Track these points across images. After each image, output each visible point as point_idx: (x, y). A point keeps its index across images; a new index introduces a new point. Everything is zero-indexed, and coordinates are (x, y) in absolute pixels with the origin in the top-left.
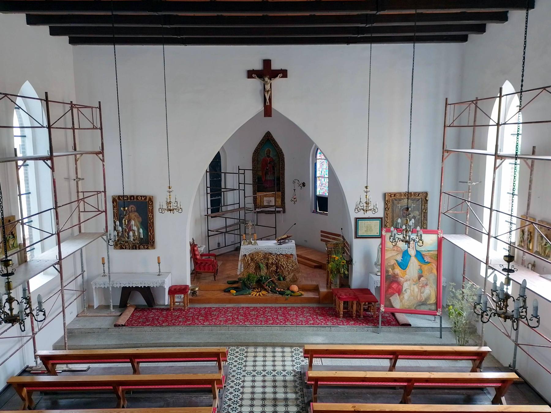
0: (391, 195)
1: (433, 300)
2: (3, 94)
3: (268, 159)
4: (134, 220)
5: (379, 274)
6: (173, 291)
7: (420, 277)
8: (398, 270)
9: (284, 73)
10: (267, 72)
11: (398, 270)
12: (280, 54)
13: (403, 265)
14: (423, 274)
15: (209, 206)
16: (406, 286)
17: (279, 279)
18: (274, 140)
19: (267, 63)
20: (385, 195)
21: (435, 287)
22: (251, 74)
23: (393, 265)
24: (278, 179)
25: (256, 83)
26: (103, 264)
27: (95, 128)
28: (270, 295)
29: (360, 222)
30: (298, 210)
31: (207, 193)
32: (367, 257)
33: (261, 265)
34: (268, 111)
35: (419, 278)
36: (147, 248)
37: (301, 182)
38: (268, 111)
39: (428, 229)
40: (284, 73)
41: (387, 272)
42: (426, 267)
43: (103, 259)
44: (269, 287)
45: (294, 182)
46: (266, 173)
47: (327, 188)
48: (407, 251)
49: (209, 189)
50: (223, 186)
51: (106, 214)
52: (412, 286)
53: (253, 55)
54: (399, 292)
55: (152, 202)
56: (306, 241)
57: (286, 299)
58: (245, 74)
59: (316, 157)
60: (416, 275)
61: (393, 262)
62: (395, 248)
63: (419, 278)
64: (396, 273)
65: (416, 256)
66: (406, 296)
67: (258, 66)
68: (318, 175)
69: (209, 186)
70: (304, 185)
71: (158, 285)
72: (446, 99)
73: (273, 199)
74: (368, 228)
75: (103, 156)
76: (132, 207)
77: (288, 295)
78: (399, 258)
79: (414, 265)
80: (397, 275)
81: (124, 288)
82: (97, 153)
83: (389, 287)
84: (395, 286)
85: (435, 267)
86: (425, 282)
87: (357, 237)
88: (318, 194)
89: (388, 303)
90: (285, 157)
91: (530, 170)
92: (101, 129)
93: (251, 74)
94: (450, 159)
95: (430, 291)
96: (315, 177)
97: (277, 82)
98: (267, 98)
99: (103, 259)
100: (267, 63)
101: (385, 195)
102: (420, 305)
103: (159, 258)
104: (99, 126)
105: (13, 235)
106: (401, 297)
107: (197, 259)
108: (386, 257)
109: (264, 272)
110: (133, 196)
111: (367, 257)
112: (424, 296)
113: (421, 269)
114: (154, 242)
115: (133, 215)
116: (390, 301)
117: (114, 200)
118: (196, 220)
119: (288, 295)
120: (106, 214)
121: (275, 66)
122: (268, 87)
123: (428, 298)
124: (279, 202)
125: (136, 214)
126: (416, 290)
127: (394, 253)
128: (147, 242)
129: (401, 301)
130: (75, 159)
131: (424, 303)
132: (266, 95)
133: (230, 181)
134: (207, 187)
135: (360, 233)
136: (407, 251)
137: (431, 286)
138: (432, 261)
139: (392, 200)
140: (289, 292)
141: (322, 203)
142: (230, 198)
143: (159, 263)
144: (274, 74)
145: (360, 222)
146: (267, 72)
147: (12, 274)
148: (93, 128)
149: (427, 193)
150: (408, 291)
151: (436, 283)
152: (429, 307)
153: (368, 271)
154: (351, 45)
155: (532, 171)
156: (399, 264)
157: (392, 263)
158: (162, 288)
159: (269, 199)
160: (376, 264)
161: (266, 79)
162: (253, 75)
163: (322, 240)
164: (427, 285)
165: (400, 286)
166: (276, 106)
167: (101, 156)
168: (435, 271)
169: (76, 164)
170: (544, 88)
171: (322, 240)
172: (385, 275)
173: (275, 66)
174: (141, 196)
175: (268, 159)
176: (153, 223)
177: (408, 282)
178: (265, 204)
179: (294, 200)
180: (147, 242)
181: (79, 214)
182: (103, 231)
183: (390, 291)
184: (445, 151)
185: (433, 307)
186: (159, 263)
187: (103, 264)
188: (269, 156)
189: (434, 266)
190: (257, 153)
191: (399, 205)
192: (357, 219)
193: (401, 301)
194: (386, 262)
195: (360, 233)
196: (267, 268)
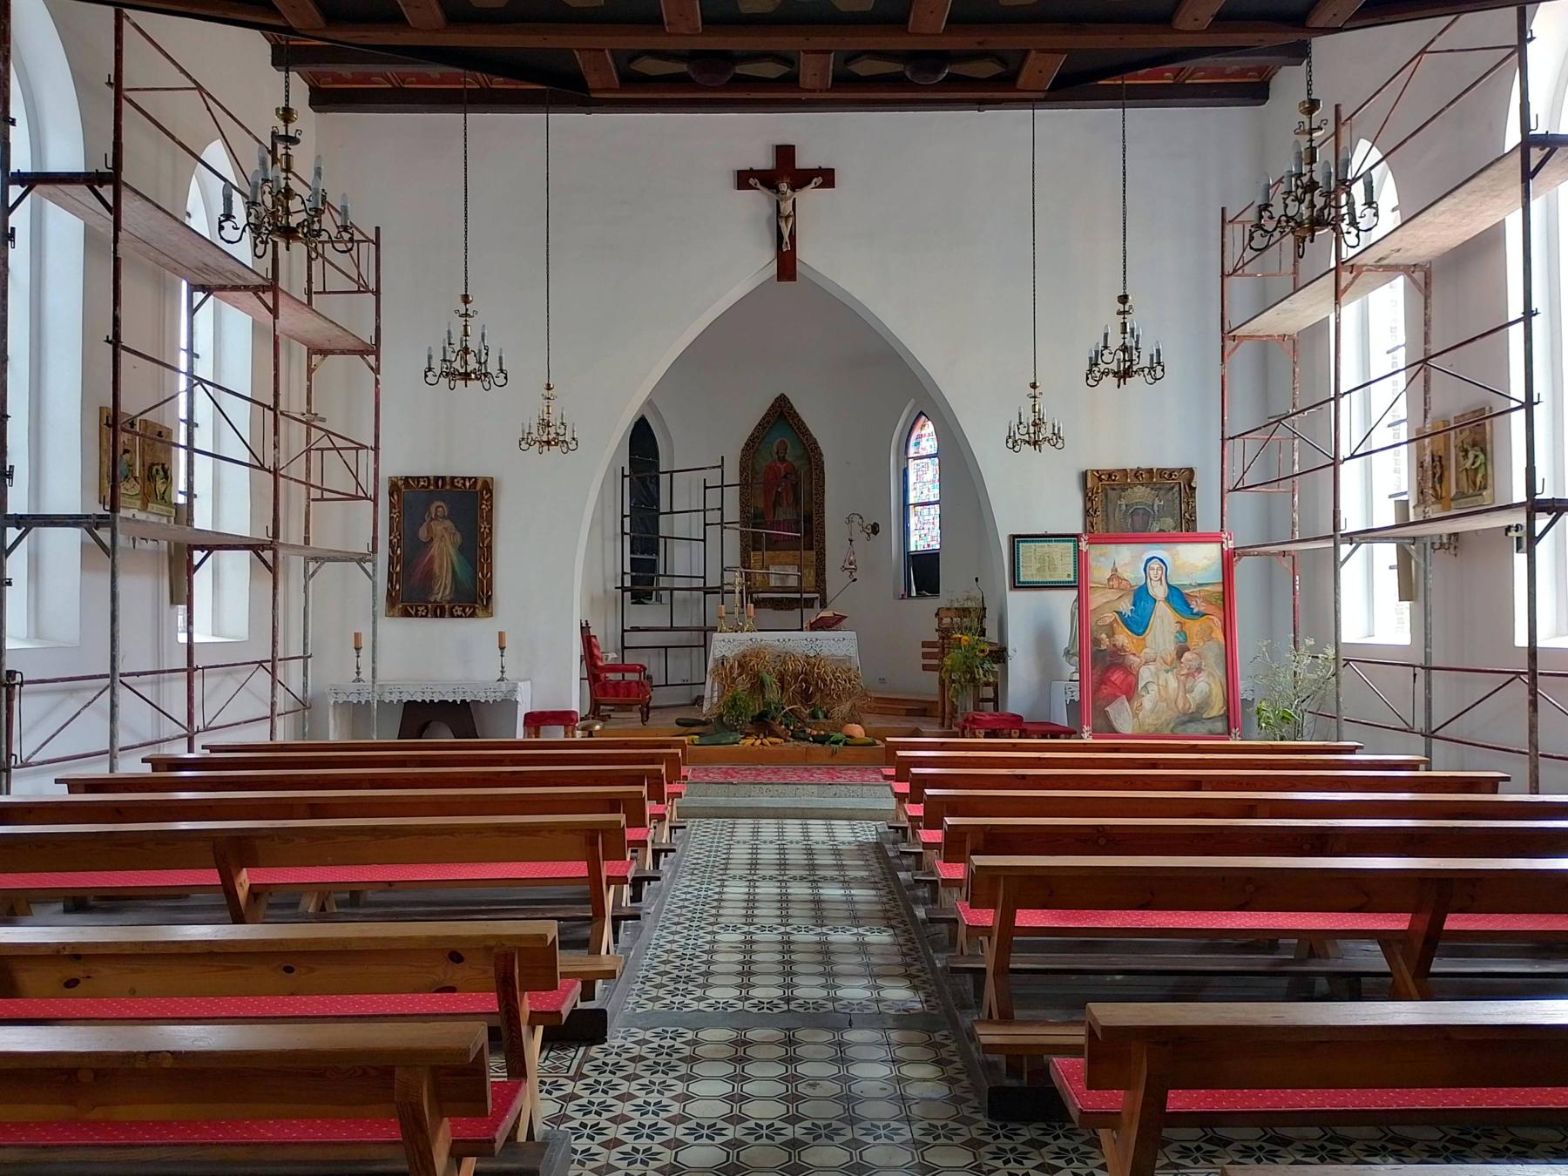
0: (1099, 475)
1: (1217, 708)
2: (195, 82)
3: (782, 467)
4: (441, 545)
5: (1077, 677)
6: (535, 720)
7: (1181, 651)
8: (1123, 638)
9: (827, 178)
10: (784, 174)
11: (1123, 638)
12: (816, 134)
13: (1138, 624)
14: (1190, 644)
15: (627, 569)
16: (1145, 674)
17: (814, 716)
18: (796, 416)
19: (785, 153)
20: (1084, 475)
21: (1220, 673)
22: (744, 179)
23: (1111, 625)
24: (808, 519)
25: (757, 201)
26: (358, 649)
27: (362, 289)
28: (792, 744)
29: (1023, 547)
30: (862, 585)
31: (623, 533)
32: (1044, 639)
33: (768, 679)
34: (787, 265)
35: (1180, 655)
36: (472, 615)
37: (869, 521)
38: (787, 265)
39: (1199, 530)
40: (827, 178)
41: (1097, 642)
42: (1194, 627)
43: (357, 636)
44: (787, 726)
45: (849, 520)
46: (776, 504)
47: (937, 531)
48: (1144, 588)
49: (627, 520)
50: (664, 507)
51: (376, 505)
52: (1163, 676)
53: (750, 135)
54: (1130, 690)
55: (491, 492)
56: (882, 680)
57: (834, 753)
58: (731, 180)
59: (906, 452)
60: (1171, 648)
61: (1110, 617)
62: (1115, 583)
63: (1180, 655)
64: (1119, 644)
65: (1167, 599)
66: (1147, 701)
67: (765, 162)
68: (912, 500)
69: (627, 512)
70: (875, 529)
71: (499, 697)
72: (1223, 209)
73: (792, 570)
74: (1046, 563)
75: (378, 359)
76: (439, 507)
77: (837, 742)
78: (1126, 606)
79: (1164, 621)
80: (1123, 648)
81: (410, 705)
82: (363, 352)
83: (1103, 681)
84: (1117, 677)
85: (1220, 624)
86: (1195, 664)
87: (1017, 585)
88: (913, 548)
89: (1100, 722)
90: (826, 459)
91: (1422, 298)
92: (377, 293)
93: (744, 179)
94: (1242, 356)
95: (1208, 686)
96: (905, 506)
97: (810, 199)
98: (786, 234)
99: (357, 636)
100: (785, 153)
101: (1084, 475)
102: (1184, 723)
103: (501, 634)
104: (372, 286)
105: (165, 472)
106: (1136, 704)
107: (596, 666)
108: (1092, 606)
109: (773, 695)
110: (443, 478)
111: (1044, 639)
112: (1195, 698)
113: (1182, 632)
114: (489, 598)
115: (438, 527)
116: (1106, 715)
117: (394, 488)
118: (592, 599)
119: (837, 742)
120: (376, 505)
121: (803, 161)
122: (786, 207)
123: (1204, 704)
124: (810, 578)
125: (448, 523)
126: (1173, 684)
127: (1112, 595)
128: (473, 597)
129: (1136, 715)
130: (309, 366)
131: (1193, 717)
132: (783, 225)
133: (683, 496)
134: (624, 516)
135: (1025, 575)
136: (1144, 588)
137: (1210, 674)
138: (1211, 609)
139: (1105, 490)
140: (838, 736)
141: (924, 572)
142: (681, 560)
143: (502, 648)
144: (802, 179)
145: (1023, 547)
146: (784, 174)
147: (295, 141)
148: (359, 291)
149: (1191, 471)
150: (1153, 688)
151: (1222, 665)
152: (1209, 726)
153: (1048, 672)
154: (990, 114)
155: (1426, 298)
156: (1127, 622)
157: (1108, 621)
158: (510, 704)
159: (783, 573)
160: (1067, 653)
161: (784, 187)
162: (752, 181)
163: (925, 667)
164: (1199, 670)
165: (1130, 678)
166: (806, 254)
167: (371, 359)
168: (1219, 635)
169: (309, 379)
170: (1423, 51)
171: (925, 667)
172: (1089, 649)
173: (803, 161)
174: (464, 478)
175: (782, 467)
176: (490, 547)
177: (1152, 667)
178: (773, 582)
179: (850, 568)
180: (473, 597)
181: (308, 506)
182: (363, 547)
183: (1106, 690)
184: (1226, 334)
185: (1220, 726)
186: (502, 648)
187: (358, 649)
188: (782, 460)
189: (1217, 621)
190: (752, 447)
191: (1123, 502)
192: (1015, 539)
193: (1136, 715)
194: (1093, 619)
195: (1025, 575)
196: (782, 688)
